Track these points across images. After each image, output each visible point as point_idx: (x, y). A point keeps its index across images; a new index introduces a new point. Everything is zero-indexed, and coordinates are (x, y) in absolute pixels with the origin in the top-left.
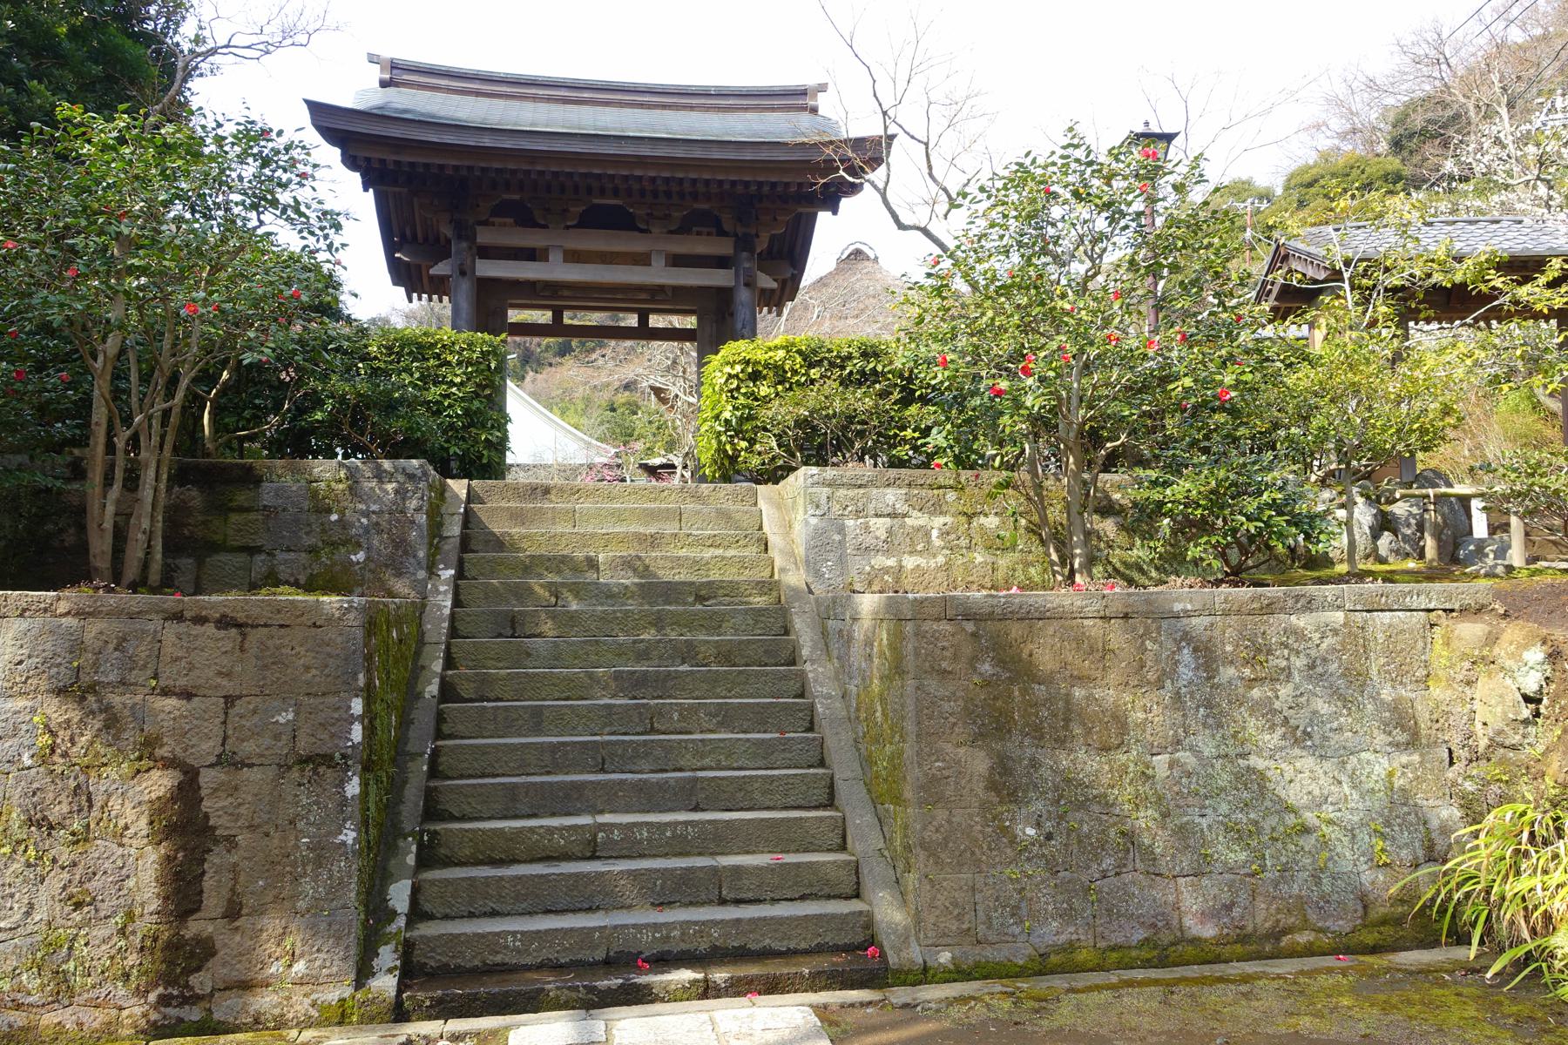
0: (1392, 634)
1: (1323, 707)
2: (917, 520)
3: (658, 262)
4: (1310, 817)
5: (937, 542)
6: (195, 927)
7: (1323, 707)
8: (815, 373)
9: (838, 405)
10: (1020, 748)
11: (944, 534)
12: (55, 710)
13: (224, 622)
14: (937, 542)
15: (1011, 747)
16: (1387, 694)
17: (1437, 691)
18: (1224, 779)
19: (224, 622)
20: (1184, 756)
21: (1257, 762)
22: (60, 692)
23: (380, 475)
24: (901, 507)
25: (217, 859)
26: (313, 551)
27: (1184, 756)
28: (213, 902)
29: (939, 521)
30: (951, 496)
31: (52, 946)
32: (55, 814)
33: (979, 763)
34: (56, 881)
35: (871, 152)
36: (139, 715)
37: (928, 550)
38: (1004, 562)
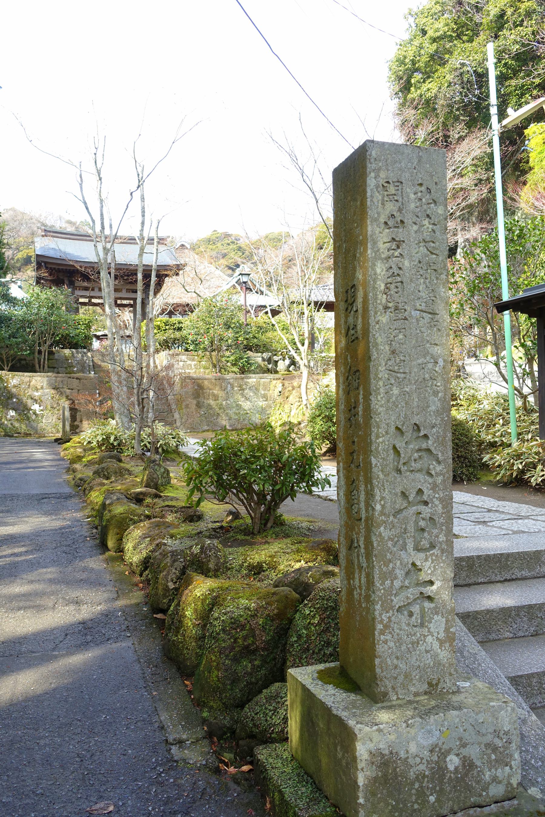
0: (264, 383)
1: (251, 394)
2: (189, 362)
3: (124, 291)
4: (248, 412)
5: (193, 367)
6: (76, 423)
7: (251, 394)
8: (167, 327)
9: (172, 336)
10: (201, 399)
11: (195, 365)
12: (53, 391)
13: (77, 379)
14: (193, 367)
15: (200, 400)
16: (263, 392)
17: (271, 392)
18: (234, 405)
19: (77, 379)
20: (228, 402)
21: (240, 403)
22: (54, 389)
23: (77, 353)
24: (186, 360)
25: (78, 413)
26: (66, 368)
27: (228, 402)
28: (78, 420)
29: (193, 363)
30: (196, 357)
31: (56, 425)
32: (55, 406)
33: (195, 402)
34: (56, 416)
35: (185, 265)
36: (65, 392)
37: (191, 369)
38: (207, 371)
